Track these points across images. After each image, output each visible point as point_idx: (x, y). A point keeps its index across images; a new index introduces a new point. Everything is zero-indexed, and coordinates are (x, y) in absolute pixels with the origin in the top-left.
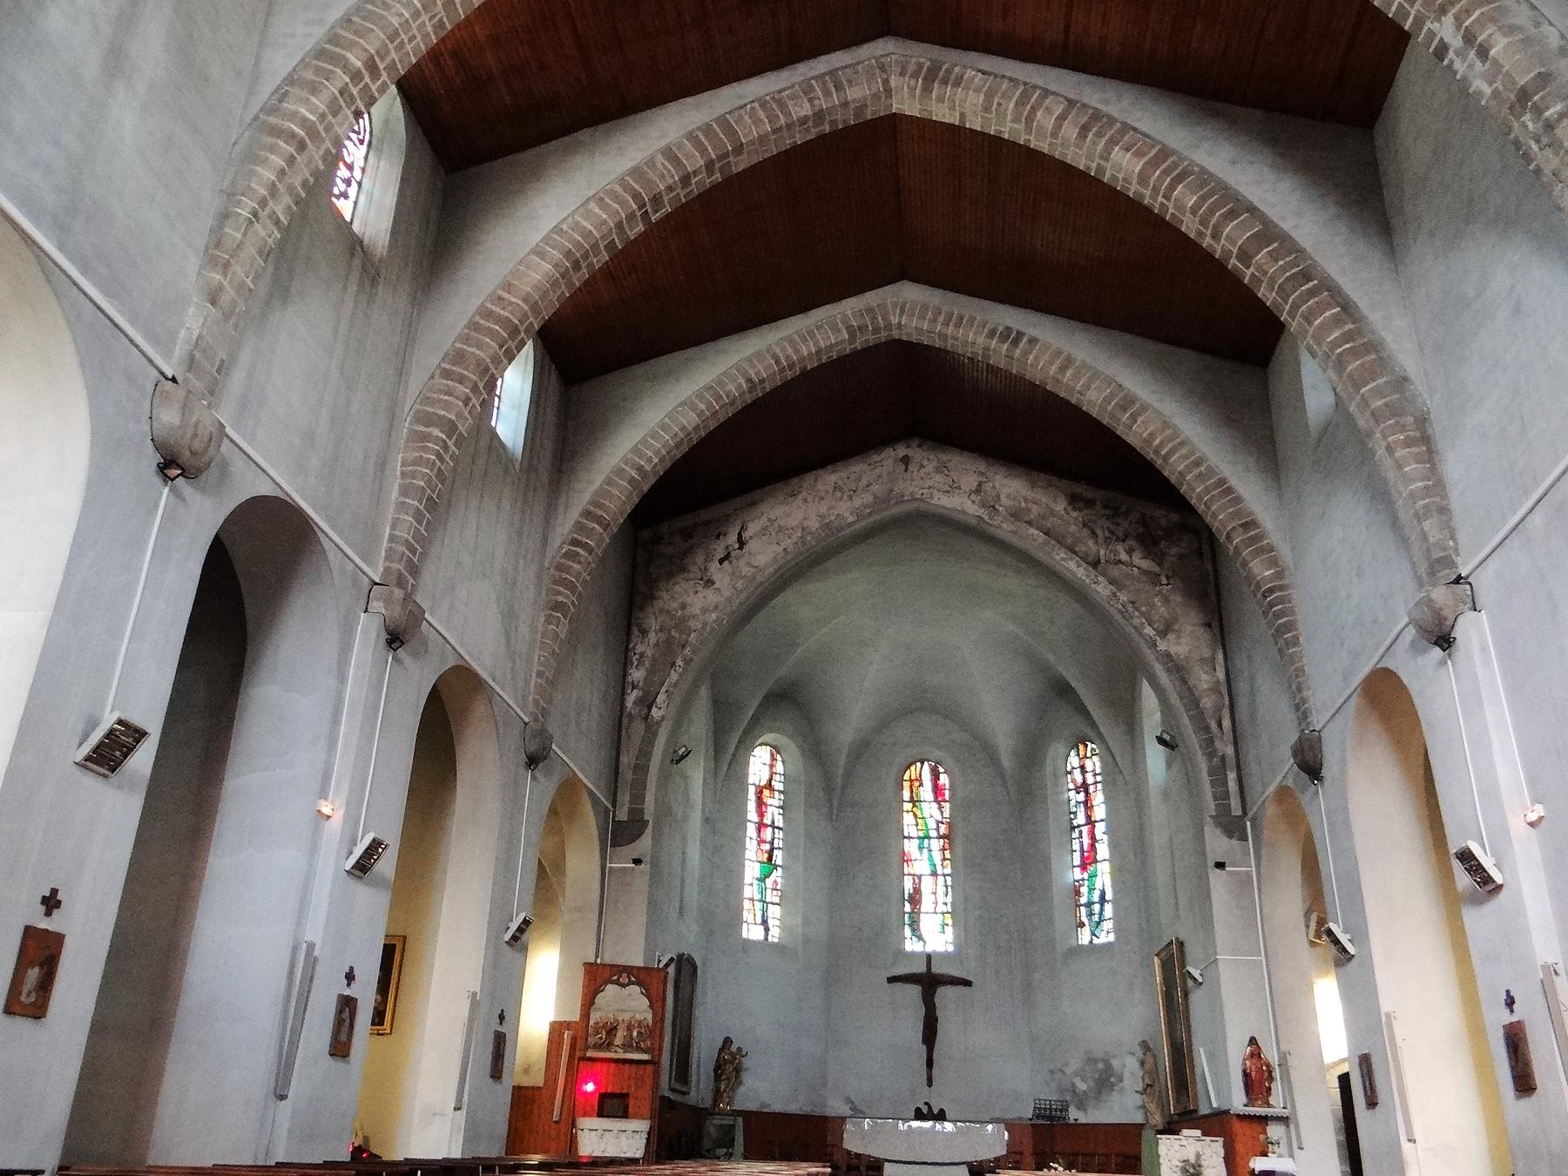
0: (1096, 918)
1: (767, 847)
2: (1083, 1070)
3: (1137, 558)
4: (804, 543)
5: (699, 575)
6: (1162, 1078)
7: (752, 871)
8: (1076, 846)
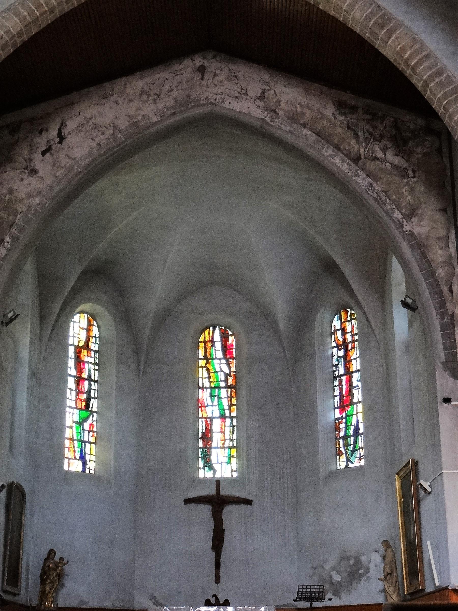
0: (351, 448)
1: (84, 396)
2: (339, 564)
3: (390, 156)
4: (115, 138)
5: (25, 165)
6: (399, 568)
7: (71, 416)
8: (337, 392)
